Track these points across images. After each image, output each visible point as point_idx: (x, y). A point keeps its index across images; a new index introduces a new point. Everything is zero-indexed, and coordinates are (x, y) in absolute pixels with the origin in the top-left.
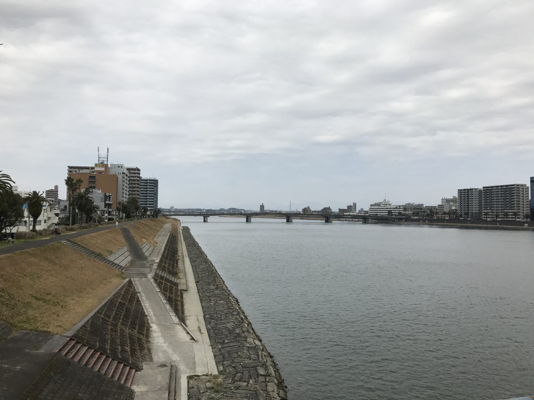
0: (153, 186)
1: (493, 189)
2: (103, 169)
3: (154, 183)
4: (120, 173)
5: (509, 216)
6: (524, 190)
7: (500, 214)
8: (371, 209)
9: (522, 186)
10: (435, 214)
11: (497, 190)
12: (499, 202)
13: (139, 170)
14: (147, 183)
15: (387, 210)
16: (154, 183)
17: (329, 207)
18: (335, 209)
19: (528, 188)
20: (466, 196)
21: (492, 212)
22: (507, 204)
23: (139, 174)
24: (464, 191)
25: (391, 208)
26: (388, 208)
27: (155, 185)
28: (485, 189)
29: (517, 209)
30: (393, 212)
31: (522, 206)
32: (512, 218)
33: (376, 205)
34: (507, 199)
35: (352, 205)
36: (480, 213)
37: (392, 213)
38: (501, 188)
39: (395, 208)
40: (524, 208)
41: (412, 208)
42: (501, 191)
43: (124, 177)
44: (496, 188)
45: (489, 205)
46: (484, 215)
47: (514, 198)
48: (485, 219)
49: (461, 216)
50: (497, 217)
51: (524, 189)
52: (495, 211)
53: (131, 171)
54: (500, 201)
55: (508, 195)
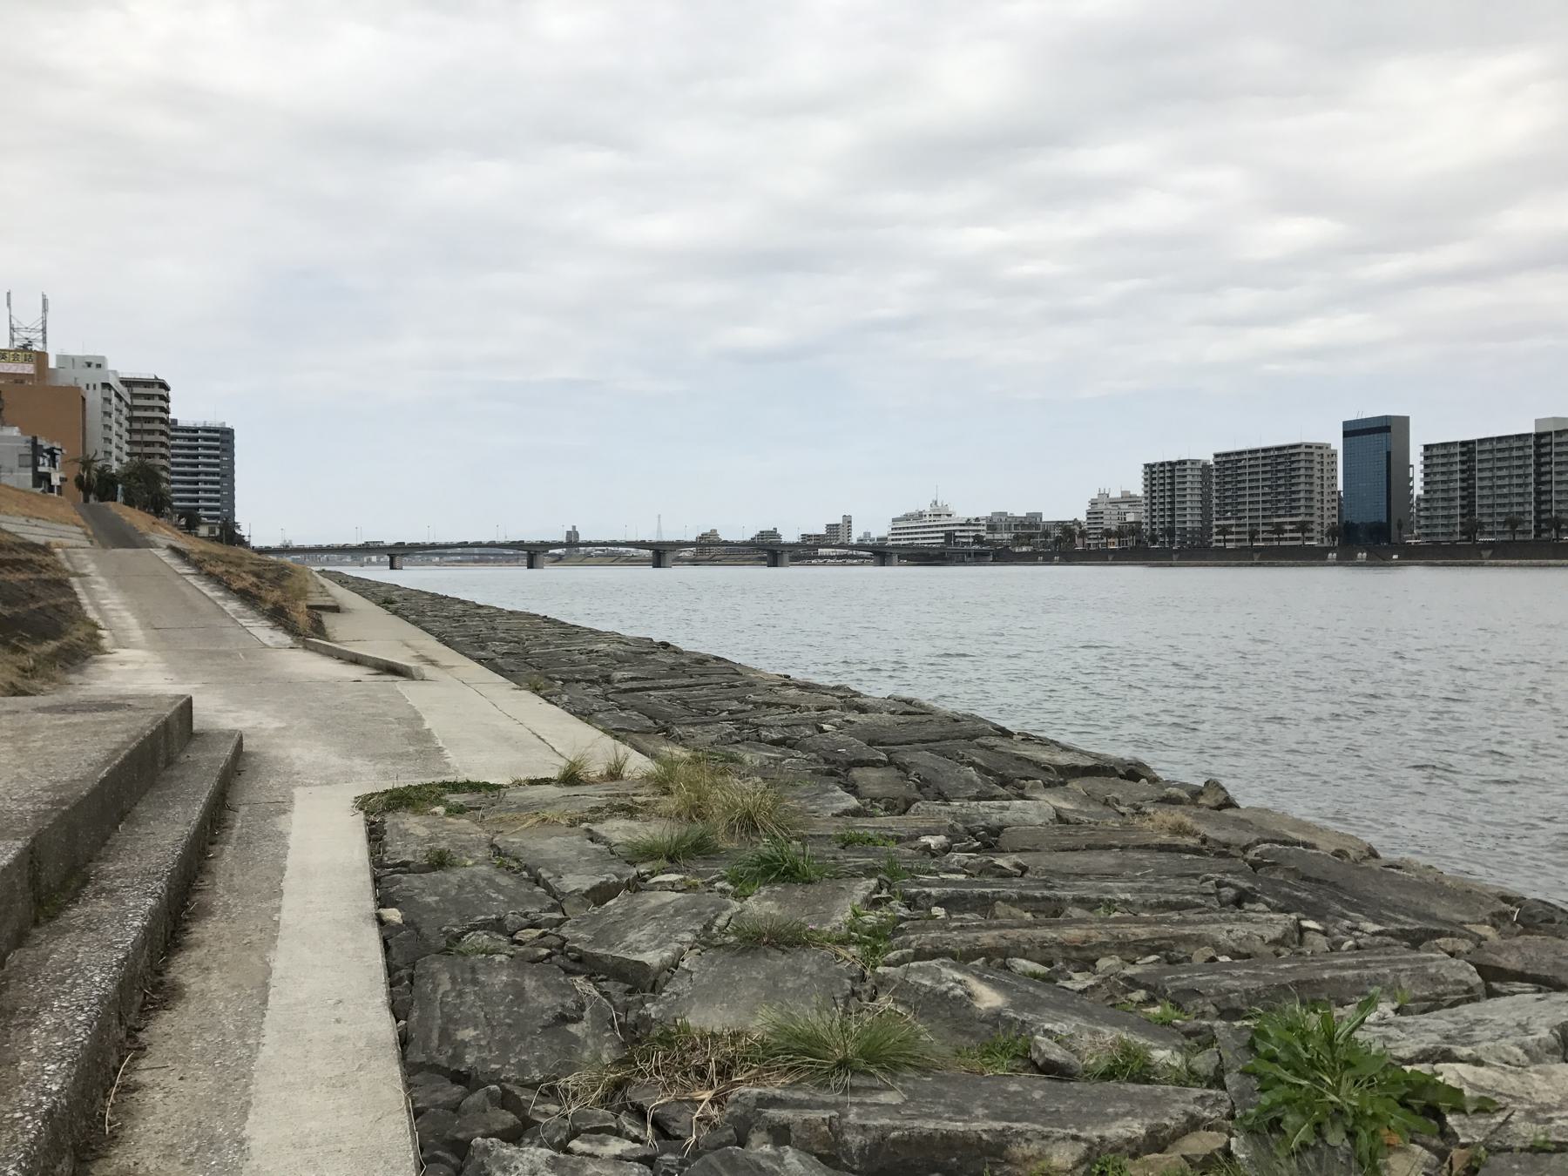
0: (216, 448)
1: (1240, 461)
2: (29, 369)
3: (222, 439)
4: (95, 386)
5: (1286, 535)
6: (1326, 460)
7: (1261, 528)
8: (896, 529)
9: (1320, 448)
10: (1079, 537)
11: (1252, 462)
12: (1258, 495)
13: (164, 386)
14: (196, 439)
15: (942, 531)
16: (222, 439)
17: (775, 529)
18: (790, 536)
19: (1334, 454)
20: (1168, 481)
21: (1238, 525)
22: (1279, 501)
23: (167, 411)
24: (1162, 469)
25: (954, 525)
26: (945, 525)
27: (225, 446)
28: (1219, 459)
29: (1306, 514)
30: (960, 537)
31: (1319, 505)
32: (1292, 539)
33: (907, 518)
34: (1280, 486)
35: (840, 521)
36: (1206, 530)
37: (957, 540)
38: (1263, 454)
39: (963, 525)
40: (1322, 503)
41: (1010, 525)
42: (1264, 465)
43: (108, 400)
44: (1250, 456)
45: (1231, 475)
46: (1217, 534)
47: (1300, 483)
48: (1222, 544)
49: (1154, 539)
50: (1252, 539)
51: (1325, 456)
52: (1247, 521)
53: (137, 390)
54: (1260, 491)
55: (1282, 474)
